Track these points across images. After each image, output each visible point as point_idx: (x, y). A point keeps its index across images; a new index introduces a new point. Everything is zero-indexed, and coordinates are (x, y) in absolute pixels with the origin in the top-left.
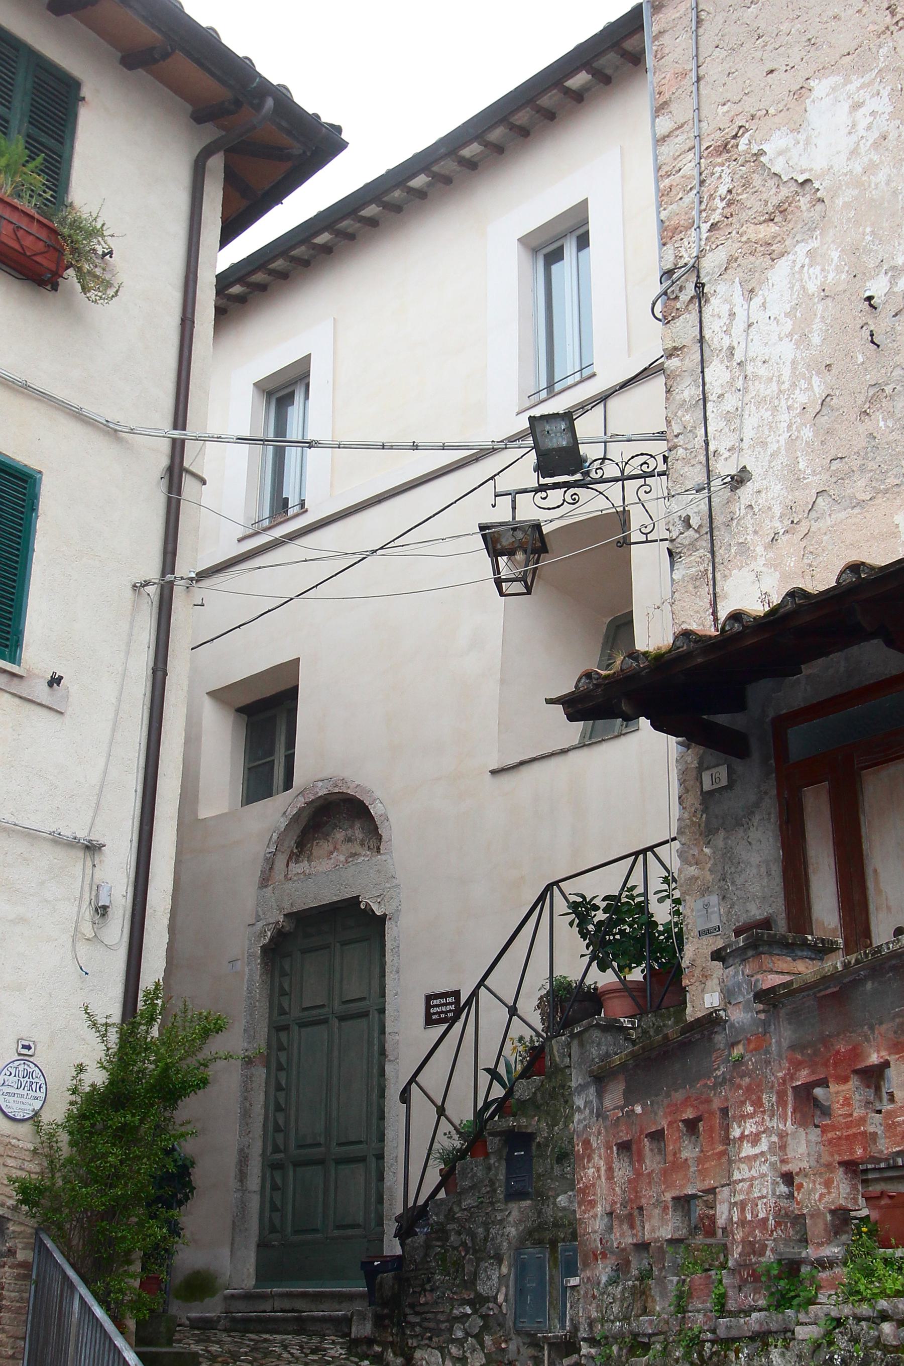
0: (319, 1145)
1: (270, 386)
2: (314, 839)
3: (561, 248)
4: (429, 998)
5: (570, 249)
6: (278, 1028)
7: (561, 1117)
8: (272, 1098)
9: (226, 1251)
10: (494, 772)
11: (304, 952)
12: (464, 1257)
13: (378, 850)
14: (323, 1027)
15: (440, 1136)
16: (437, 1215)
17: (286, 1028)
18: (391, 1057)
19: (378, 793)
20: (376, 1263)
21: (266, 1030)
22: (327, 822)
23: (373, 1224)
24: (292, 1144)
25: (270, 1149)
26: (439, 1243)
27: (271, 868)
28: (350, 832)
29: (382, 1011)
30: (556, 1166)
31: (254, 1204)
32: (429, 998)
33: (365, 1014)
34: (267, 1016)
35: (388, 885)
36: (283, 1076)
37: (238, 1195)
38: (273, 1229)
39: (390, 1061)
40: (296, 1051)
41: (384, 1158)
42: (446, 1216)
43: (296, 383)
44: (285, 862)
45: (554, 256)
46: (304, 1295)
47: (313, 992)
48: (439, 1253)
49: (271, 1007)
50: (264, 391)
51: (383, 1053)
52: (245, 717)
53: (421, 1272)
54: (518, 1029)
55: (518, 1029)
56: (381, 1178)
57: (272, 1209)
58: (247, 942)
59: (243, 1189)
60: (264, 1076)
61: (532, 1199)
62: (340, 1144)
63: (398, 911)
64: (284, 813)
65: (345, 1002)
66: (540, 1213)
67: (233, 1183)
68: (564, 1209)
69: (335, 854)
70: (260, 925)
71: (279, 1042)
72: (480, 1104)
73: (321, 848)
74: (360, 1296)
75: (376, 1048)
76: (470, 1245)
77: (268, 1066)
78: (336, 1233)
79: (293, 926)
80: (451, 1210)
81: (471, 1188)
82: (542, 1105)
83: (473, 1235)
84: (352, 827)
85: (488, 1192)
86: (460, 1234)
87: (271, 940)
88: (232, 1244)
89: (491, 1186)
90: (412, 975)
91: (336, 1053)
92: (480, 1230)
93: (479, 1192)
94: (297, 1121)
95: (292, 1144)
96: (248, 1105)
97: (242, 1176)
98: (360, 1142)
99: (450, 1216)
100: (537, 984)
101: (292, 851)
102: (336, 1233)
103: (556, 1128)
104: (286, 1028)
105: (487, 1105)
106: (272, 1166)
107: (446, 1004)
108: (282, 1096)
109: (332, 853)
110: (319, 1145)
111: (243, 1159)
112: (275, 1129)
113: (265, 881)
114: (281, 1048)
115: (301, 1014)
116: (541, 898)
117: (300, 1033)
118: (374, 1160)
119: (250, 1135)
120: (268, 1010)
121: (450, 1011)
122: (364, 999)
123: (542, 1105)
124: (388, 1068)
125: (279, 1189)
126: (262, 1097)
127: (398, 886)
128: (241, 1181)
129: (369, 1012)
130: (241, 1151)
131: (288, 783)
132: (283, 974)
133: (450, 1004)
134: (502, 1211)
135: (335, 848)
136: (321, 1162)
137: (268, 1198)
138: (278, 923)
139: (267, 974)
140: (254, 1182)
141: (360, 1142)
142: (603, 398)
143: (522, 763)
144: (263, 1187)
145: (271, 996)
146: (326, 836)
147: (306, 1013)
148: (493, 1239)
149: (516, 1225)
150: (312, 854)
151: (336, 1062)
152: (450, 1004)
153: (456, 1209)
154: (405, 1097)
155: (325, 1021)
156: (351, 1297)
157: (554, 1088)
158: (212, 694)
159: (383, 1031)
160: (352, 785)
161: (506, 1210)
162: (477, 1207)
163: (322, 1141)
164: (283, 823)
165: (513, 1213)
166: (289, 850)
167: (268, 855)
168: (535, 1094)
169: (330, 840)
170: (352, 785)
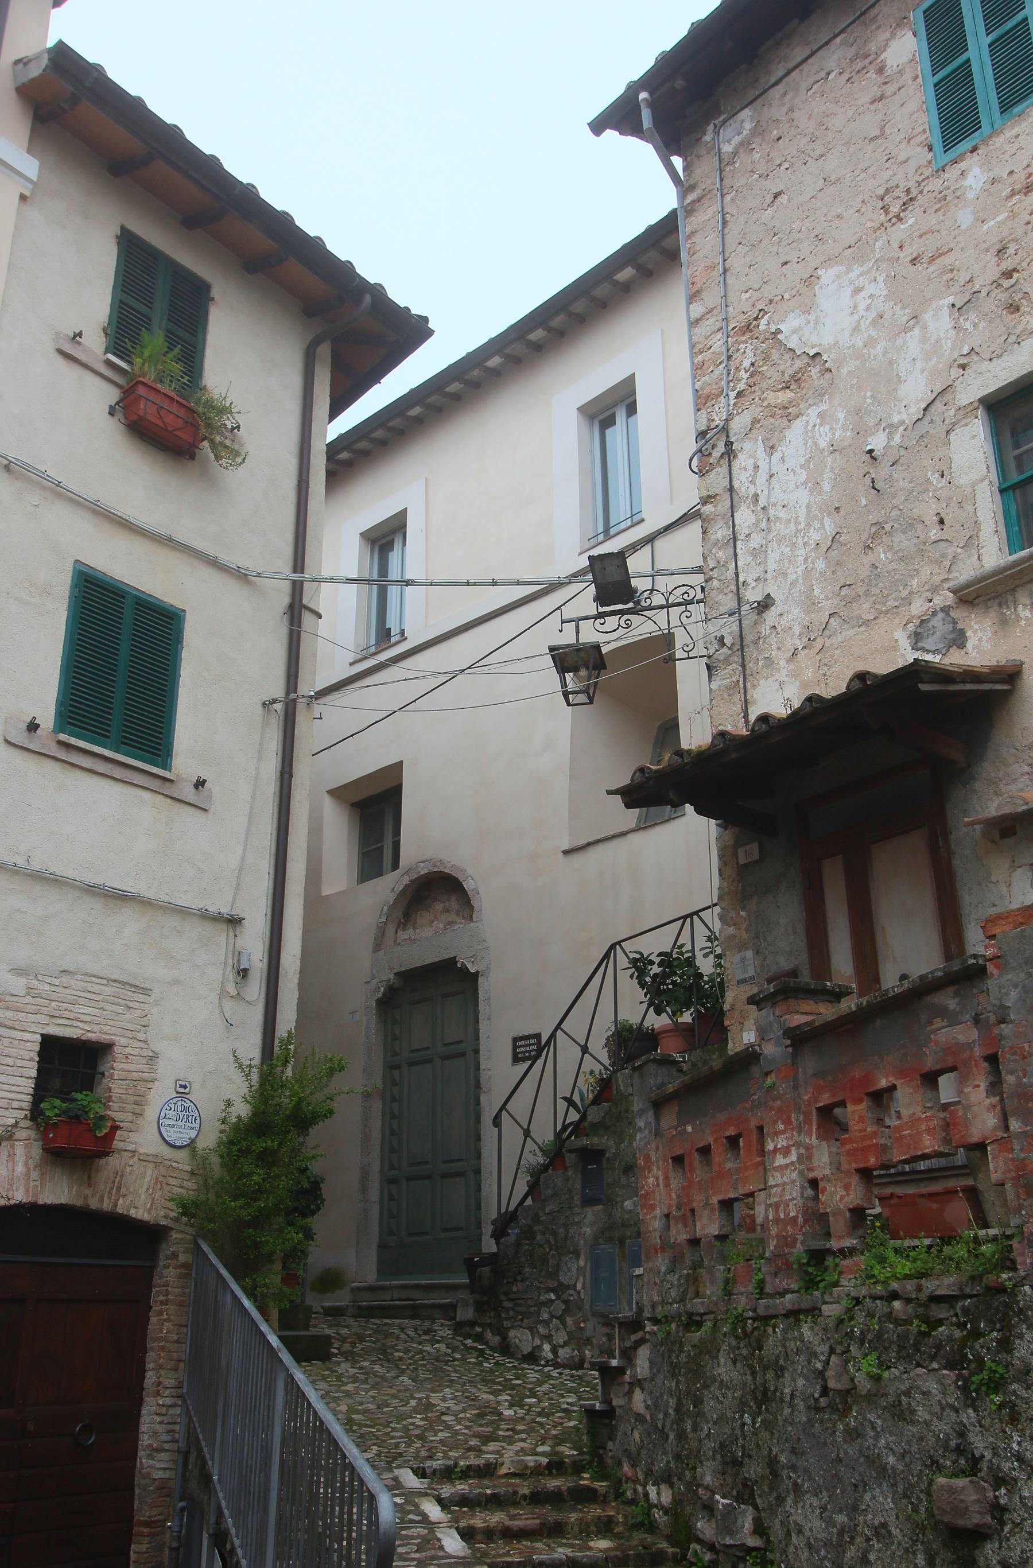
0: (426, 1163)
3: (614, 414)
4: (515, 1040)
5: (621, 416)
6: (391, 1067)
10: (566, 852)
13: (471, 919)
19: (469, 872)
28: (447, 904)
29: (477, 1051)
32: (515, 1040)
33: (463, 1054)
45: (608, 422)
51: (478, 1085)
55: (589, 1063)
62: (445, 1162)
63: (488, 968)
65: (413, 1051)
70: (374, 982)
73: (423, 917)
75: (472, 1082)
80: (536, 1214)
83: (555, 1235)
87: (384, 994)
90: (498, 1027)
92: (561, 1230)
97: (364, 1189)
99: (536, 1220)
100: (604, 1028)
104: (397, 1067)
105: (565, 1127)
106: (389, 1181)
111: (365, 1174)
113: (377, 947)
114: (394, 1084)
116: (607, 956)
121: (533, 1050)
122: (461, 1042)
128: (363, 1193)
129: (466, 1052)
131: (396, 865)
133: (533, 1044)
135: (436, 917)
136: (429, 1177)
140: (374, 1194)
148: (572, 1238)
152: (533, 1044)
153: (541, 1213)
154: (497, 1121)
155: (429, 1061)
158: (332, 793)
160: (448, 866)
168: (604, 1117)
170: (448, 866)
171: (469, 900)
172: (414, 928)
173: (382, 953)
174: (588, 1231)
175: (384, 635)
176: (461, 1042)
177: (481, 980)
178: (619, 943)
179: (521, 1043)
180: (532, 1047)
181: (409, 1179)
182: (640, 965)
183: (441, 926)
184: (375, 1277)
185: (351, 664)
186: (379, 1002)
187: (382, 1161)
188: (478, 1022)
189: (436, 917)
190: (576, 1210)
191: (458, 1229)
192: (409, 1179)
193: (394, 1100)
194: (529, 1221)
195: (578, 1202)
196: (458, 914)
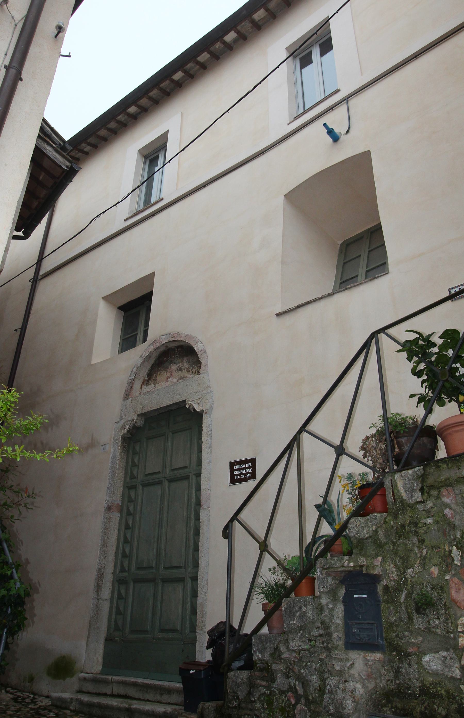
0: (151, 568)
1: (146, 153)
3: (310, 53)
4: (233, 464)
5: (316, 53)
6: (129, 487)
7: (416, 558)
8: (122, 534)
9: (84, 643)
10: (278, 315)
12: (295, 706)
13: (199, 373)
15: (264, 571)
16: (262, 652)
18: (204, 506)
19: (199, 338)
20: (192, 672)
21: (122, 488)
22: (167, 360)
23: (187, 631)
24: (133, 568)
25: (118, 569)
26: (264, 683)
27: (131, 388)
28: (180, 365)
29: (199, 475)
30: (416, 617)
31: (106, 607)
32: (233, 464)
33: (187, 478)
34: (123, 479)
35: (204, 392)
38: (117, 628)
39: (203, 509)
40: (139, 503)
41: (197, 580)
42: (272, 655)
43: (160, 150)
44: (140, 385)
45: (306, 61)
46: (135, 685)
47: (152, 464)
48: (264, 694)
49: (126, 474)
50: (143, 156)
51: (198, 504)
52: (123, 313)
53: (244, 712)
54: (348, 466)
55: (348, 466)
56: (195, 595)
57: (117, 611)
58: (113, 433)
60: (118, 519)
61: (384, 653)
62: (166, 568)
63: (211, 408)
64: (141, 356)
66: (397, 672)
68: (435, 674)
69: (171, 378)
70: (122, 422)
71: (129, 496)
72: (309, 539)
73: (162, 376)
74: (177, 691)
75: (193, 500)
76: (300, 691)
77: (121, 512)
78: (161, 635)
79: (143, 422)
80: (276, 649)
81: (300, 628)
82: (386, 543)
83: (305, 683)
84: (182, 362)
85: (321, 636)
86: (288, 677)
87: (128, 431)
88: (88, 638)
89: (325, 629)
90: (219, 451)
91: (166, 503)
92: (314, 678)
93: (309, 633)
94: (138, 549)
95: (133, 568)
96: (106, 538)
97: (98, 588)
98: (180, 567)
99: (276, 654)
100: (367, 422)
101: (144, 379)
102: (161, 635)
103: (410, 571)
104: (134, 487)
105: (314, 540)
106: (120, 582)
107: (245, 468)
109: (169, 378)
112: (123, 555)
113: (127, 396)
116: (366, 346)
118: (189, 580)
120: (124, 476)
121: (249, 473)
122: (186, 467)
123: (386, 543)
124: (203, 514)
125: (123, 598)
126: (116, 533)
127: (212, 392)
128: (98, 591)
129: (190, 476)
130: (99, 569)
131: (145, 340)
132: (135, 453)
133: (249, 468)
134: (340, 660)
135: (171, 375)
137: (115, 605)
138: (133, 420)
139: (124, 453)
140: (106, 593)
141: (180, 567)
142: (346, 99)
143: (299, 307)
144: (112, 597)
146: (165, 369)
148: (331, 692)
149: (361, 681)
150: (156, 380)
151: (165, 511)
152: (249, 468)
153: (282, 648)
154: (227, 533)
155: (160, 483)
156: (169, 691)
157: (403, 526)
158: (105, 298)
159: (199, 489)
160: (183, 336)
161: (347, 660)
162: (308, 650)
163: (154, 565)
164: (139, 361)
165: (357, 665)
166: (142, 379)
168: (376, 531)
169: (168, 370)
170: (183, 336)
171: (198, 358)
172: (155, 384)
173: (130, 400)
174: (360, 689)
175: (147, 203)
178: (383, 330)
179: (238, 467)
180: (248, 471)
182: (417, 349)
183: (175, 380)
184: (100, 668)
185: (125, 220)
186: (124, 438)
187: (115, 566)
188: (201, 452)
189: (171, 375)
190: (339, 654)
191: (174, 631)
192: (136, 581)
194: (267, 656)
195: (341, 643)
196: (188, 371)
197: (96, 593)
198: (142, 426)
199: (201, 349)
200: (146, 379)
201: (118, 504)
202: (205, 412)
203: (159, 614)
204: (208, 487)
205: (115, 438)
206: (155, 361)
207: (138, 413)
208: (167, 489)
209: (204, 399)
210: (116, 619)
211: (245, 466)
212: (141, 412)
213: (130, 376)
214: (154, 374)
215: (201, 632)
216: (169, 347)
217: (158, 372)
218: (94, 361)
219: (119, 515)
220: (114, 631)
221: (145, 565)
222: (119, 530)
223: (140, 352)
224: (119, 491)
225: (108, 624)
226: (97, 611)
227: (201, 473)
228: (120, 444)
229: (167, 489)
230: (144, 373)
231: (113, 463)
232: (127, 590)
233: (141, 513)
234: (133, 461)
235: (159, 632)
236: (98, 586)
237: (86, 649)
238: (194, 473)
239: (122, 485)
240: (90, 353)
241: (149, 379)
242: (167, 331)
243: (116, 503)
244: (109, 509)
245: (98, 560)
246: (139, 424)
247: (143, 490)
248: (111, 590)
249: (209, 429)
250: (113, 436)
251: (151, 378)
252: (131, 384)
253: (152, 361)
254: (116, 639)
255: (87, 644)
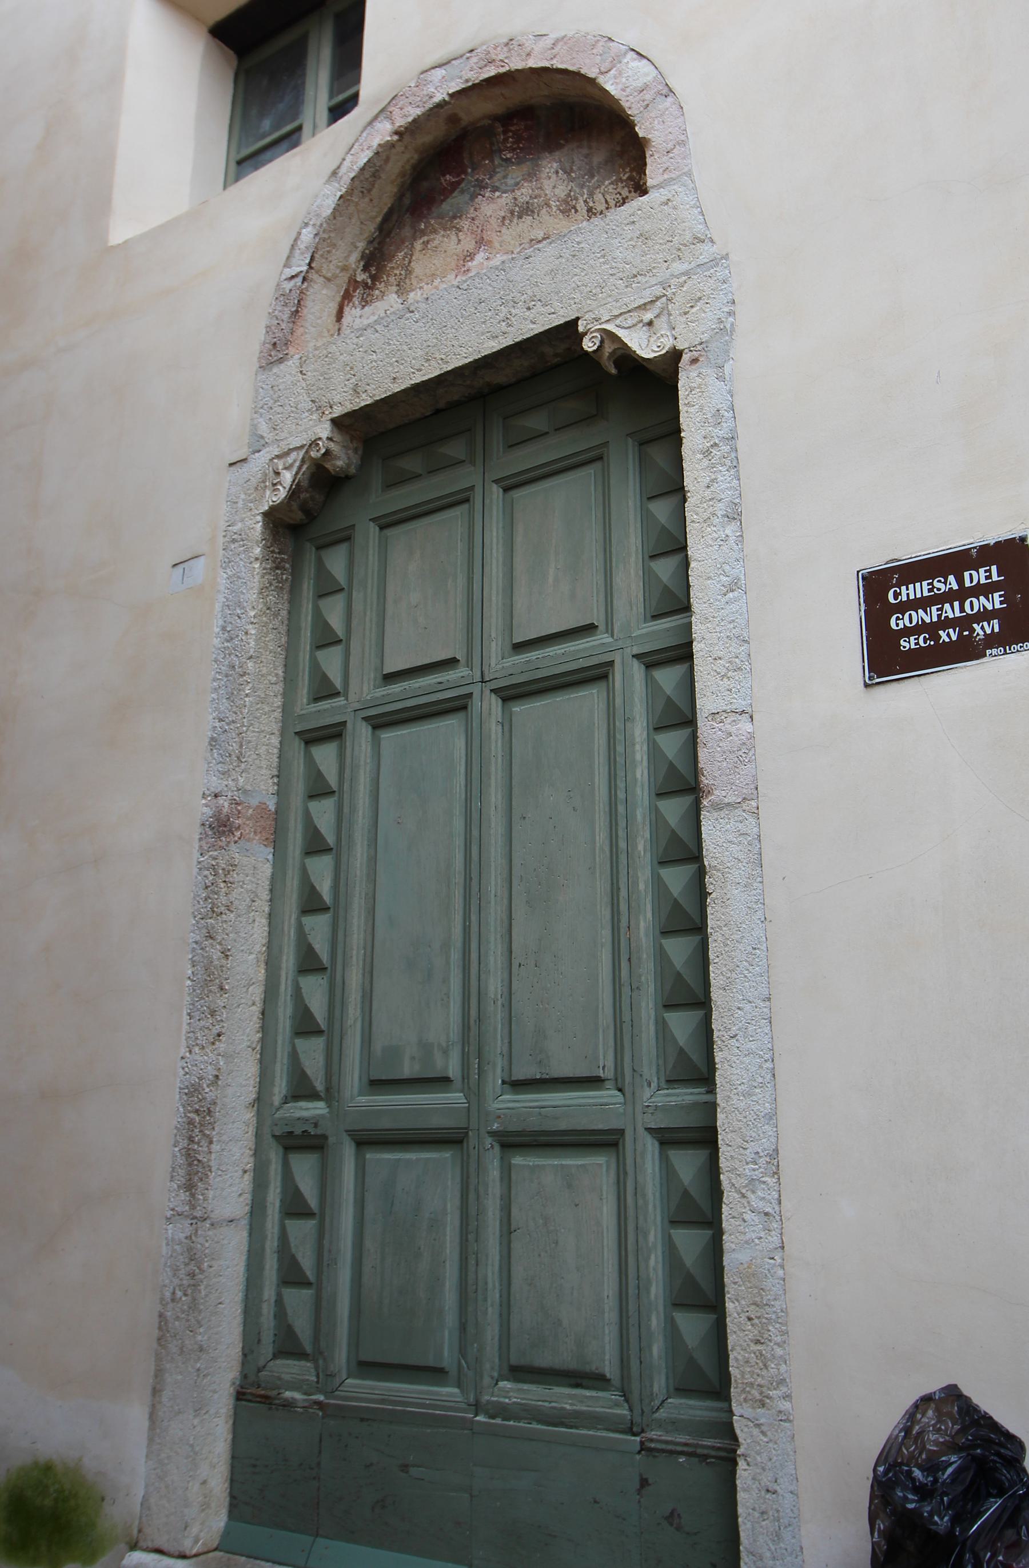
0: (443, 1082)
2: (417, 234)
4: (876, 586)
9: (137, 1415)
11: (386, 523)
13: (642, 190)
14: (452, 723)
17: (334, 733)
21: (275, 741)
24: (352, 1078)
25: (280, 1087)
28: (524, 193)
32: (876, 586)
34: (278, 702)
35: (678, 267)
36: (321, 869)
37: (180, 1230)
44: (333, 307)
49: (289, 680)
59: (197, 1218)
60: (267, 870)
63: (724, 331)
64: (334, 173)
65: (519, 647)
67: (165, 1193)
69: (480, 257)
70: (262, 458)
77: (277, 840)
78: (511, 1392)
87: (294, 493)
88: (156, 1392)
91: (495, 796)
94: (368, 997)
95: (352, 1078)
96: (216, 954)
97: (193, 1173)
98: (594, 1082)
104: (334, 733)
107: (962, 594)
108: (318, 927)
109: (471, 256)
110: (443, 1082)
111: (199, 1118)
113: (277, 350)
114: (319, 790)
115: (381, 692)
117: (376, 744)
119: (221, 1046)
120: (279, 688)
121: (985, 615)
122: (589, 629)
125: (309, 1214)
126: (258, 932)
128: (189, 1187)
130: (192, 1091)
132: (327, 589)
133: (980, 590)
136: (451, 1139)
137: (271, 1243)
138: (314, 443)
140: (230, 1192)
145: (290, 651)
146: (451, 222)
147: (396, 688)
155: (458, 706)
163: (453, 1070)
166: (343, 280)
167: (288, 286)
172: (402, 290)
173: (291, 365)
176: (589, 629)
177: (687, 380)
179: (910, 592)
181: (367, 1141)
184: (219, 1521)
186: (273, 518)
192: (367, 1141)
193: (315, 845)
196: (568, 208)
197: (184, 1196)
198: (353, 470)
199: (639, 84)
200: (361, 277)
201: (262, 807)
202: (686, 358)
203: (494, 1295)
204: (740, 704)
205: (235, 528)
206: (400, 197)
207: (338, 411)
208: (494, 730)
209: (677, 299)
210: (279, 1302)
211: (960, 581)
212: (349, 407)
213: (287, 265)
214: (398, 249)
215: (763, 1416)
216: (466, 119)
217: (414, 238)
218: (119, 233)
219: (268, 853)
220: (275, 1357)
221: (407, 1070)
222: (271, 917)
223: (325, 162)
224: (262, 750)
225: (245, 1323)
226: (192, 1275)
227: (690, 644)
228: (257, 551)
229: (494, 730)
230: (348, 255)
231: (229, 634)
232: (325, 1181)
233: (373, 841)
234: (322, 626)
235: (502, 1377)
236: (190, 1165)
237: (151, 1440)
238: (636, 651)
239: (276, 727)
240: (100, 207)
241: (375, 278)
242: (457, 44)
243: (254, 802)
244: (221, 827)
245: (183, 1051)
246: (340, 463)
247: (376, 744)
248: (248, 1177)
249: (722, 432)
250: (223, 525)
251: (380, 269)
252: (295, 294)
253: (386, 194)
254: (288, 1394)
255: (152, 1417)
